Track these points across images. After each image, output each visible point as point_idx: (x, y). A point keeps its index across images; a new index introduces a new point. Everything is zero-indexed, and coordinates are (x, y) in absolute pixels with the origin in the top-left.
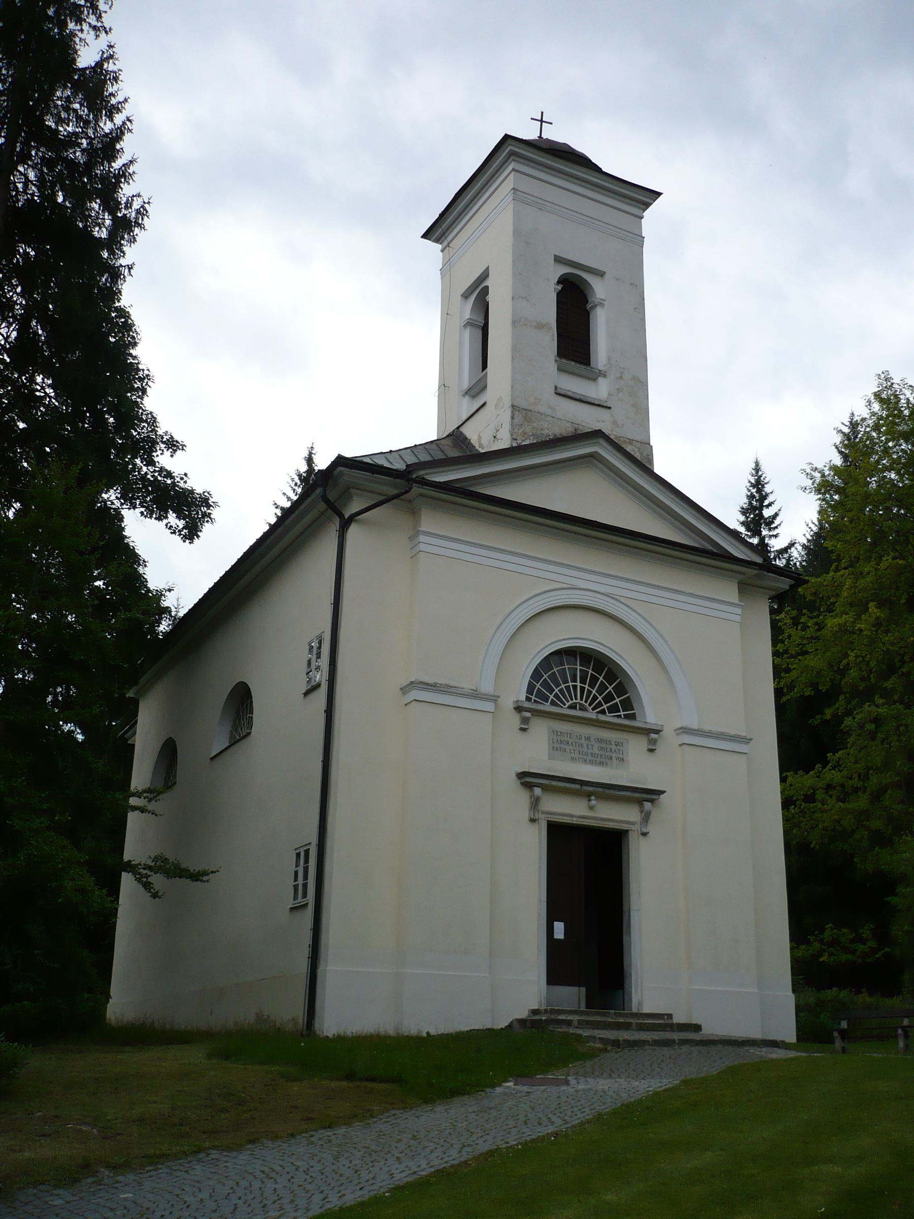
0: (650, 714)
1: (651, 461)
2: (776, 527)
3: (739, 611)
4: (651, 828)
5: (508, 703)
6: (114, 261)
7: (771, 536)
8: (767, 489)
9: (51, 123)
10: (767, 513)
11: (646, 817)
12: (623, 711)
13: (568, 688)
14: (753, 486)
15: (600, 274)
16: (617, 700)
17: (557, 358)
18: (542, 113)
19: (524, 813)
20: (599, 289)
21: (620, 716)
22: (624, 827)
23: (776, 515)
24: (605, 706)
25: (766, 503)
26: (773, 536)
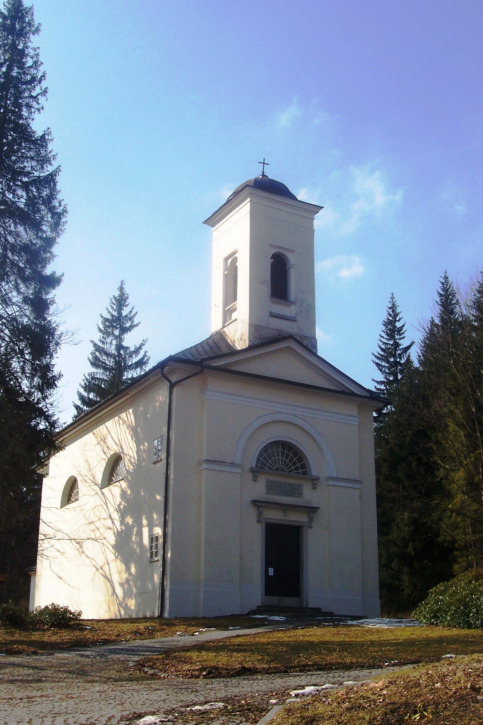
0: (314, 471)
1: (315, 347)
2: (404, 333)
3: (357, 419)
4: (314, 524)
5: (247, 467)
6: (119, 667)
7: (400, 339)
8: (398, 310)
9: (18, 21)
10: (398, 325)
11: (311, 520)
12: (301, 469)
13: (275, 460)
14: (390, 308)
15: (293, 251)
16: (299, 465)
17: (271, 298)
18: (264, 159)
19: (255, 519)
20: (292, 259)
21: (299, 473)
22: (301, 524)
23: (403, 325)
24: (293, 468)
25: (398, 319)
26: (402, 338)
